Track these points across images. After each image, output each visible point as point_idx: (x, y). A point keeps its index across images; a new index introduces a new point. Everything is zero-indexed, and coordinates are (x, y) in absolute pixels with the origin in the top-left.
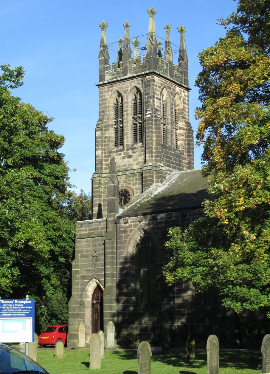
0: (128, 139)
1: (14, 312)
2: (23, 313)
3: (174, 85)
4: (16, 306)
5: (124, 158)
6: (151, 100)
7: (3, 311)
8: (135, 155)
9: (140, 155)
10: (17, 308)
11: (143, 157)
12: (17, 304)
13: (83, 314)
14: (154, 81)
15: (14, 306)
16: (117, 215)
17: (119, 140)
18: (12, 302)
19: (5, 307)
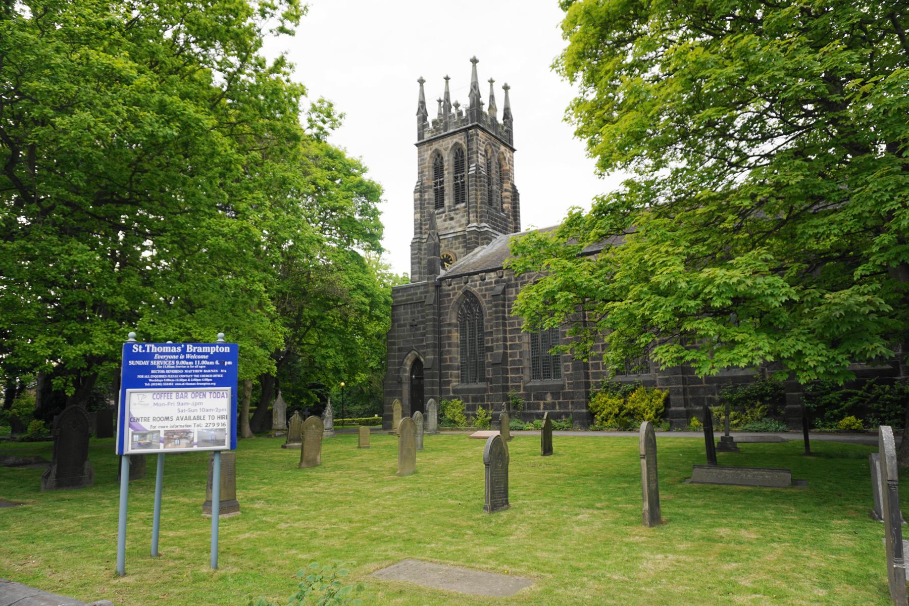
0: (448, 201)
1: (184, 373)
2: (207, 378)
3: (498, 142)
4: (189, 360)
5: (445, 220)
6: (475, 156)
7: (153, 372)
8: (457, 217)
9: (463, 216)
10: (191, 363)
11: (466, 217)
12: (192, 353)
13: (401, 392)
14: (478, 135)
15: (185, 359)
16: (439, 277)
17: (439, 203)
18: (179, 349)
19: (158, 362)
